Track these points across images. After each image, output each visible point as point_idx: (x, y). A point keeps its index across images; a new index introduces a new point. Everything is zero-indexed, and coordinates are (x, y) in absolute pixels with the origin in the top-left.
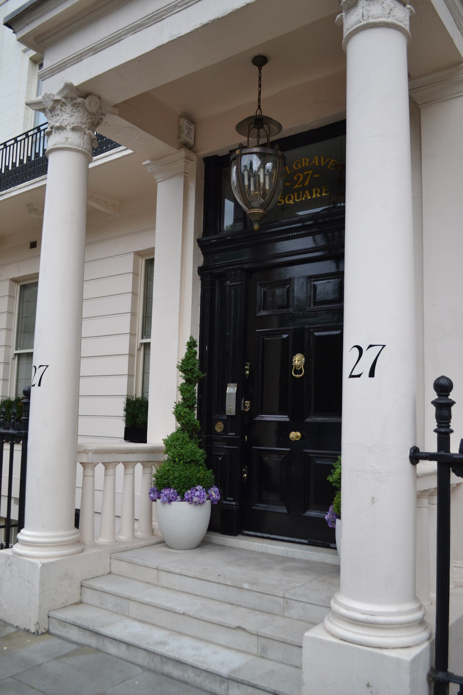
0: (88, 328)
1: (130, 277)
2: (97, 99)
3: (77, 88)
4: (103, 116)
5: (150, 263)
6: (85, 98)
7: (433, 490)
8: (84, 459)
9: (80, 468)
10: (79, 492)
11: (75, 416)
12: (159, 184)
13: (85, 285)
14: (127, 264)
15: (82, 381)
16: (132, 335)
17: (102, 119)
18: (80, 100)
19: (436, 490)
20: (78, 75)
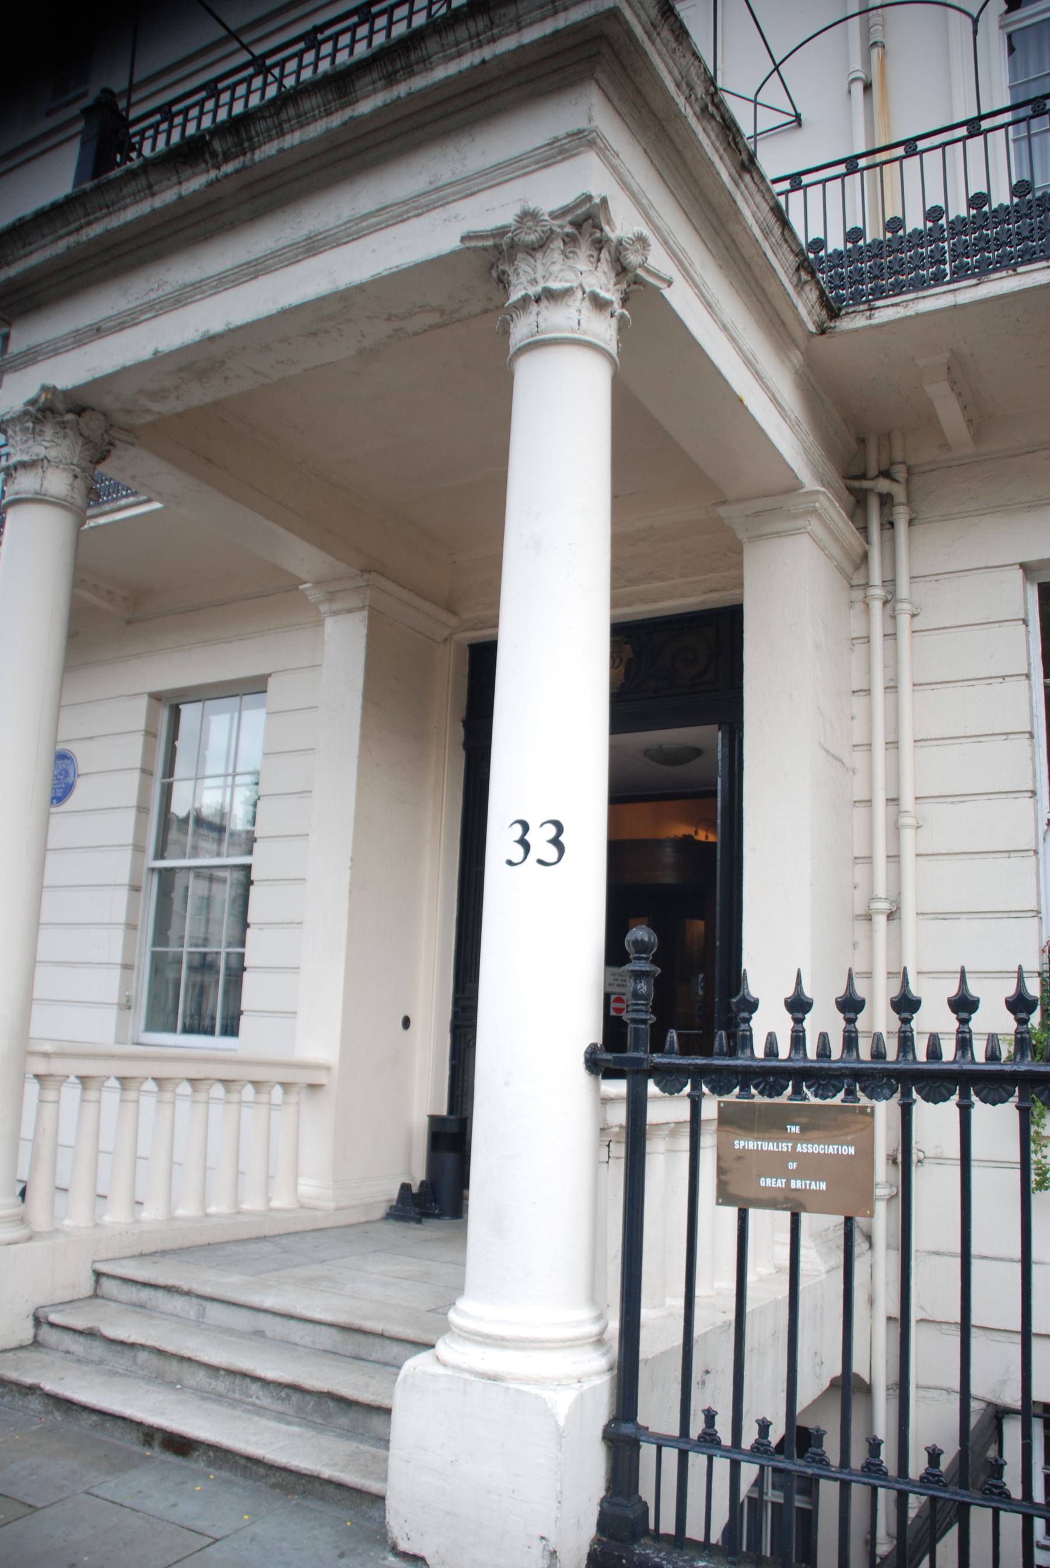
0: (50, 945)
1: (139, 740)
2: (102, 418)
3: (65, 393)
4: (111, 447)
5: (249, 882)
6: (79, 415)
7: (617, 1129)
8: (40, 1066)
9: (32, 1088)
10: (25, 1149)
11: (28, 1000)
12: (12, 517)
13: (50, 856)
14: (135, 714)
15: (36, 1010)
16: (138, 848)
17: (109, 451)
18: (70, 417)
19: (624, 1132)
20: (68, 372)
